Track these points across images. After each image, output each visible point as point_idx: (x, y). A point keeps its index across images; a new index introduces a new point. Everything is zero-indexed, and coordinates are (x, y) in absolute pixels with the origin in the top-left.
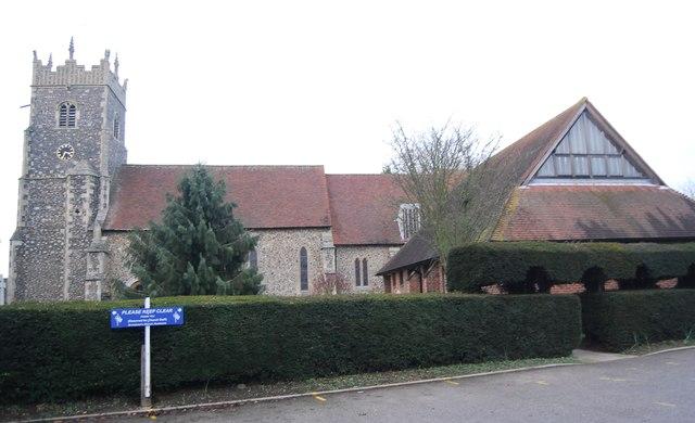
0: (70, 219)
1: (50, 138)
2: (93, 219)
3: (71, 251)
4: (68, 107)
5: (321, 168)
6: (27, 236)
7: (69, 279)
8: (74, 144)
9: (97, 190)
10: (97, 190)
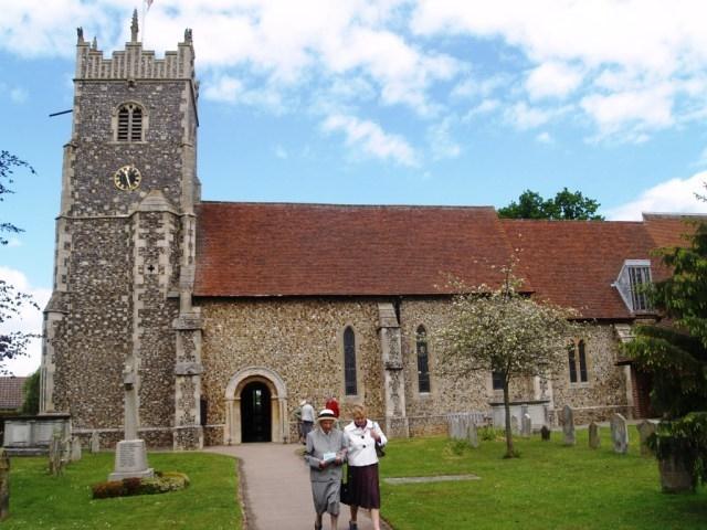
8: (140, 166)
9: (178, 237)
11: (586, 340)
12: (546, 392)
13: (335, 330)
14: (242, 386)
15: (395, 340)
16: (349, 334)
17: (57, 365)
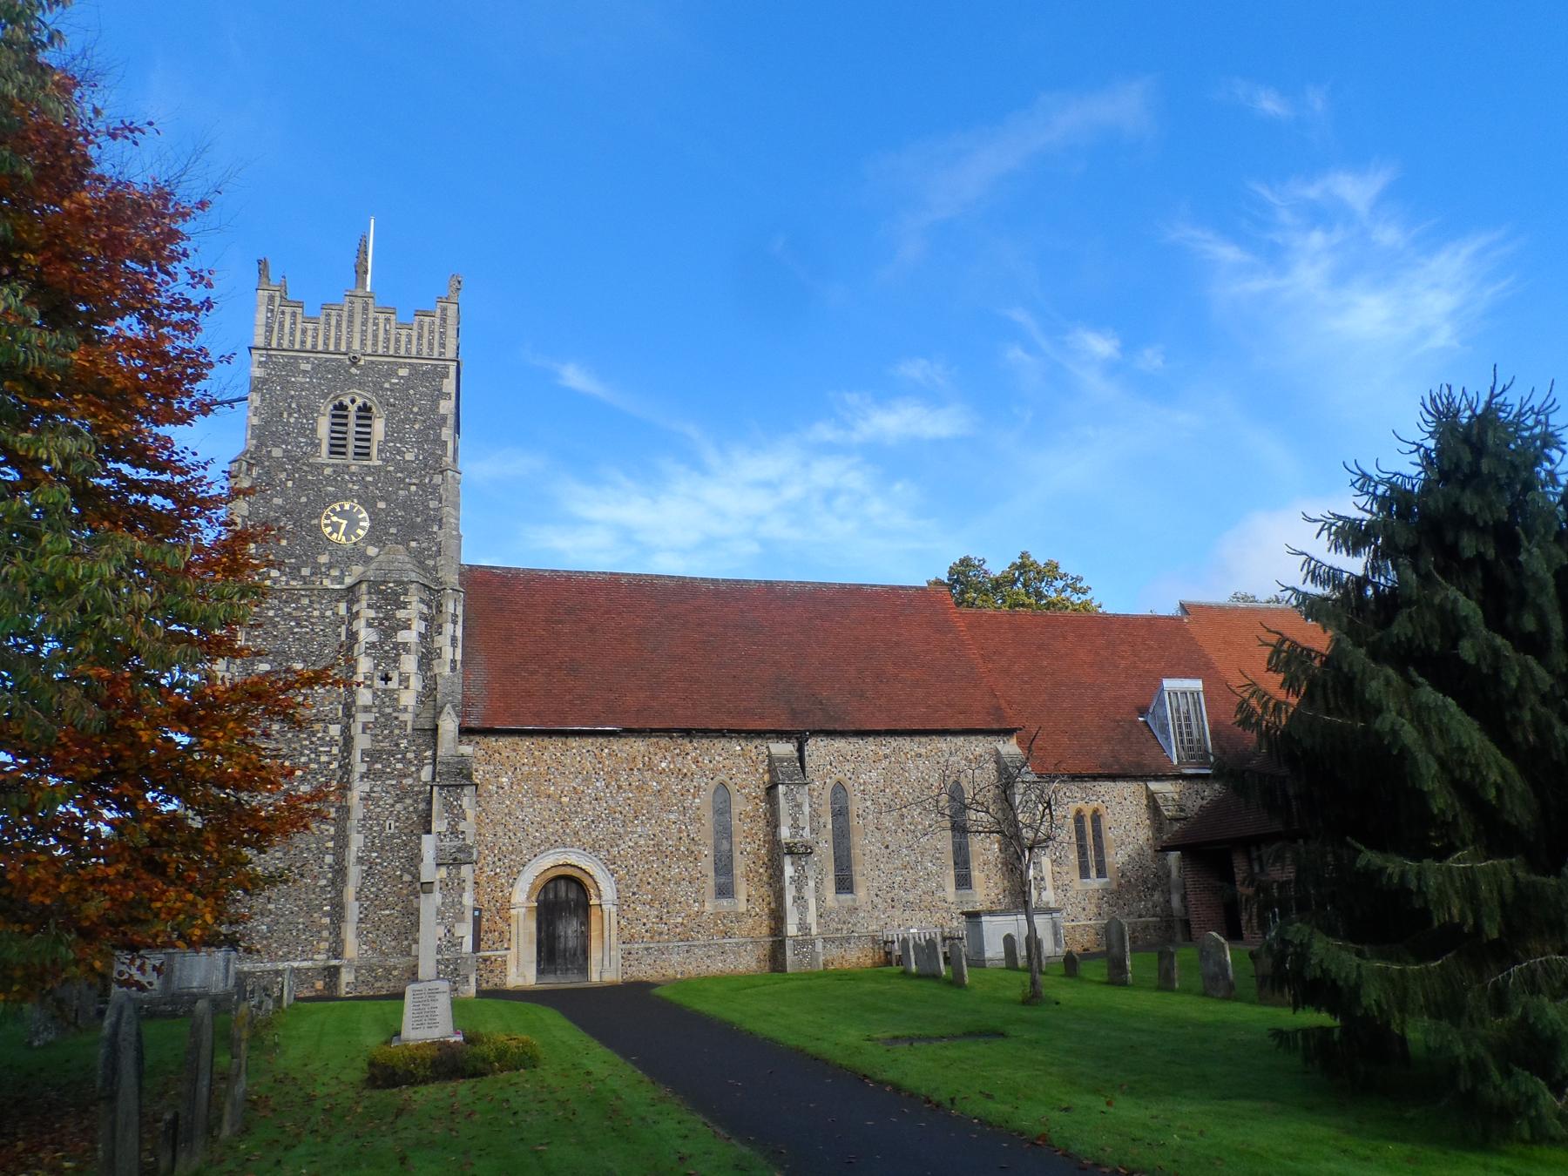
1: (301, 486)
2: (429, 692)
4: (353, 408)
7: (360, 860)
11: (1103, 810)
12: (1044, 894)
15: (799, 806)
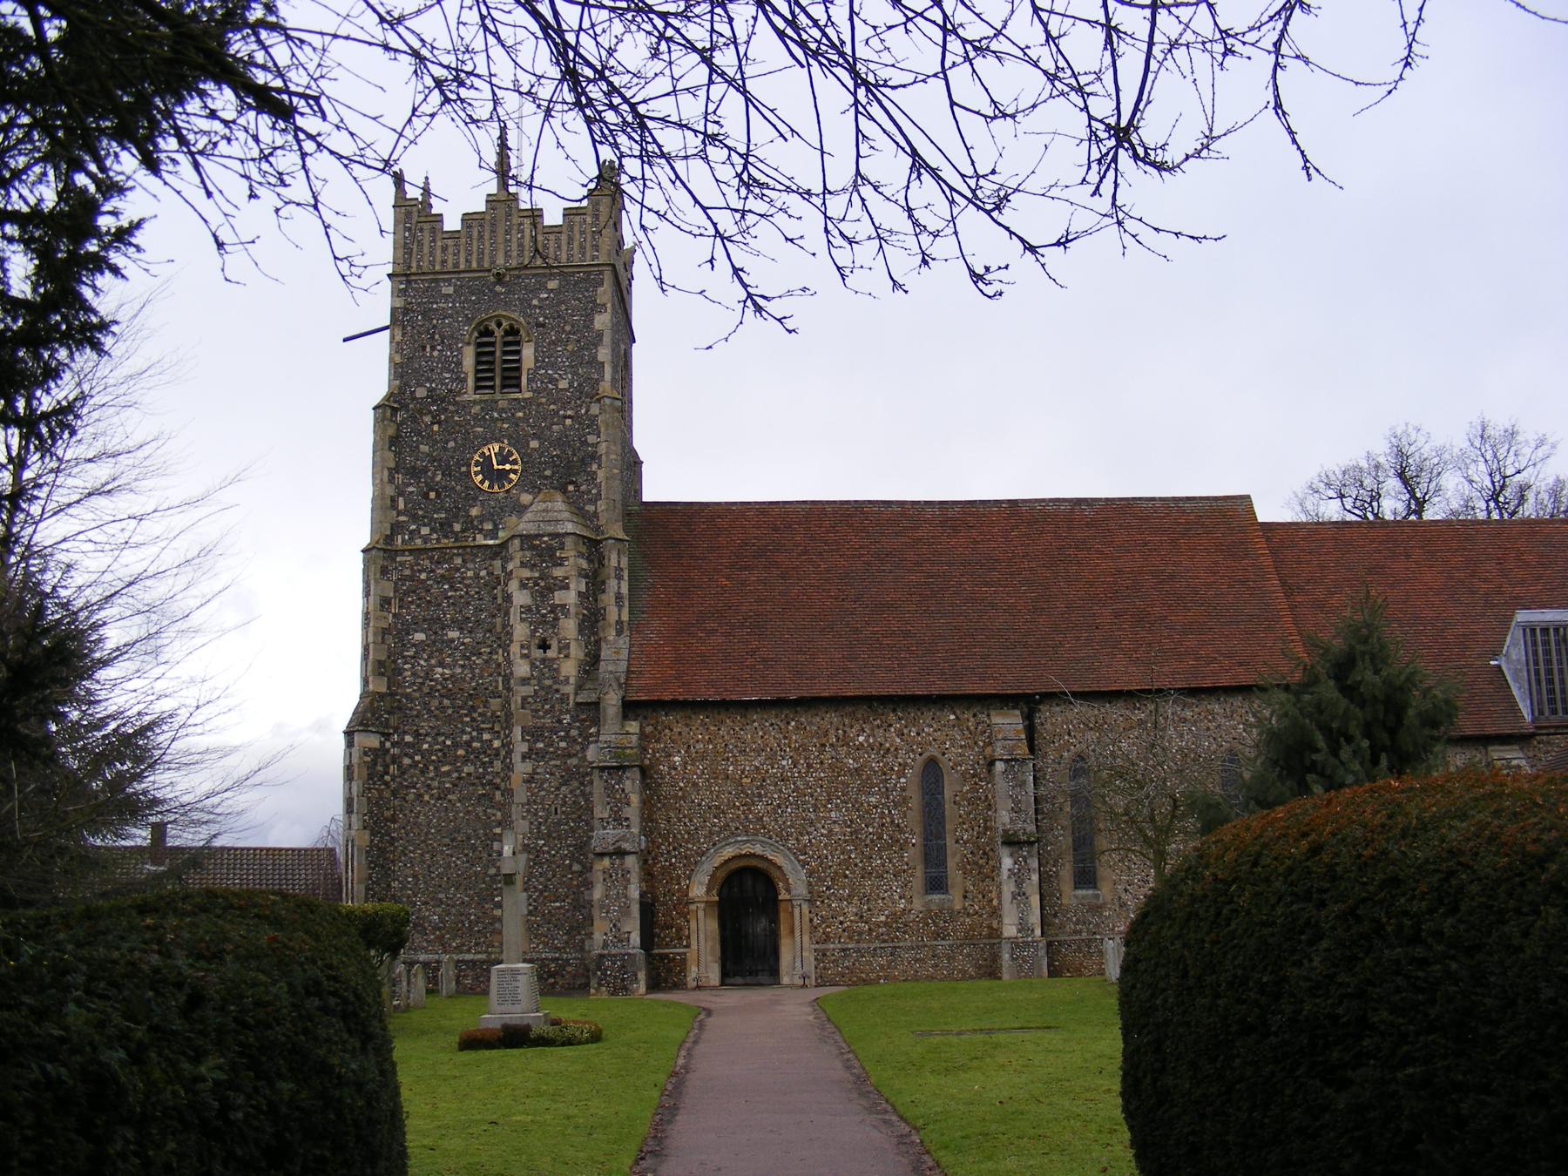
0: (522, 669)
2: (592, 661)
3: (528, 767)
4: (499, 333)
5: (1239, 506)
6: (394, 720)
8: (519, 443)
9: (595, 582)
10: (595, 582)
13: (904, 766)
14: (722, 874)
16: (932, 769)
17: (373, 834)
